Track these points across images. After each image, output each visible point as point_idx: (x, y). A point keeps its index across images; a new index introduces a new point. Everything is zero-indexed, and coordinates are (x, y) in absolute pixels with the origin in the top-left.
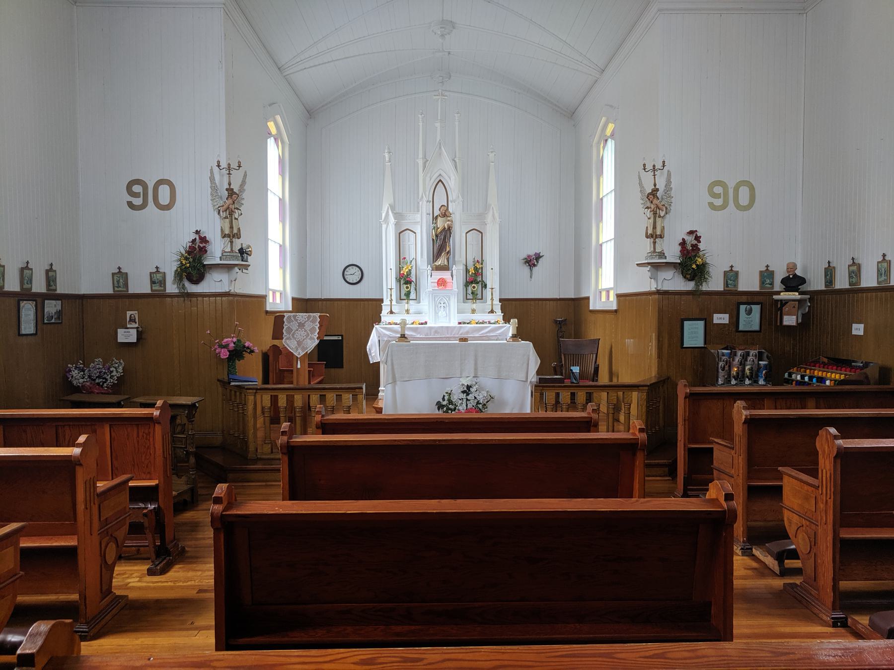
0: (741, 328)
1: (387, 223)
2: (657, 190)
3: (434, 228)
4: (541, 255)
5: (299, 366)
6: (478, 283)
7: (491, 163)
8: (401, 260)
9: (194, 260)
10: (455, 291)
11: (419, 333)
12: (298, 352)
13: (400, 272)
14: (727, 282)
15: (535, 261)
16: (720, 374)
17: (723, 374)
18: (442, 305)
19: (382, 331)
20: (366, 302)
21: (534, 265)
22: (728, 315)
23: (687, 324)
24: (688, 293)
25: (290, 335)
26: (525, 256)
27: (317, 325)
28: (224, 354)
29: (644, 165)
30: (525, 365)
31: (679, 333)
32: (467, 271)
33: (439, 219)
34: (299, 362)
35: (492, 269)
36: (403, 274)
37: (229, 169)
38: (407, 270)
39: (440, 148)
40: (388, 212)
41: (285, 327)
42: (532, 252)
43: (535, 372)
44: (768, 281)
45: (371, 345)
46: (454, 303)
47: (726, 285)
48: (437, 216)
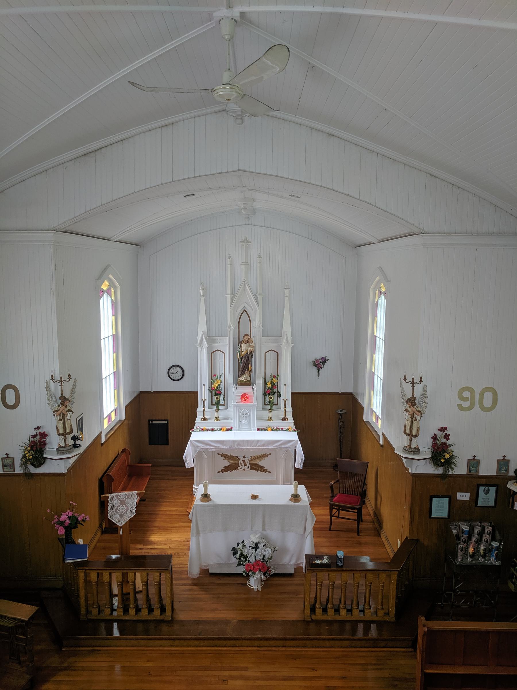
0: (480, 504)
2: (415, 399)
3: (239, 351)
5: (121, 533)
6: (273, 394)
7: (286, 298)
8: (212, 377)
9: (36, 453)
11: (225, 445)
12: (120, 522)
13: (212, 386)
14: (470, 468)
15: (321, 364)
16: (459, 553)
17: (461, 554)
18: (245, 415)
19: (195, 444)
20: (187, 394)
21: (321, 368)
22: (469, 493)
23: (434, 500)
24: (437, 476)
25: (114, 510)
26: (313, 359)
27: (134, 509)
28: (61, 532)
29: (405, 377)
30: (303, 522)
31: (428, 506)
32: (266, 383)
34: (121, 529)
35: (285, 385)
36: (214, 388)
37: (61, 382)
38: (217, 386)
39: (245, 285)
40: (202, 338)
41: (109, 505)
42: (318, 356)
43: (312, 528)
44: (504, 468)
45: (187, 455)
46: (254, 414)
47: (468, 471)
48: (242, 342)
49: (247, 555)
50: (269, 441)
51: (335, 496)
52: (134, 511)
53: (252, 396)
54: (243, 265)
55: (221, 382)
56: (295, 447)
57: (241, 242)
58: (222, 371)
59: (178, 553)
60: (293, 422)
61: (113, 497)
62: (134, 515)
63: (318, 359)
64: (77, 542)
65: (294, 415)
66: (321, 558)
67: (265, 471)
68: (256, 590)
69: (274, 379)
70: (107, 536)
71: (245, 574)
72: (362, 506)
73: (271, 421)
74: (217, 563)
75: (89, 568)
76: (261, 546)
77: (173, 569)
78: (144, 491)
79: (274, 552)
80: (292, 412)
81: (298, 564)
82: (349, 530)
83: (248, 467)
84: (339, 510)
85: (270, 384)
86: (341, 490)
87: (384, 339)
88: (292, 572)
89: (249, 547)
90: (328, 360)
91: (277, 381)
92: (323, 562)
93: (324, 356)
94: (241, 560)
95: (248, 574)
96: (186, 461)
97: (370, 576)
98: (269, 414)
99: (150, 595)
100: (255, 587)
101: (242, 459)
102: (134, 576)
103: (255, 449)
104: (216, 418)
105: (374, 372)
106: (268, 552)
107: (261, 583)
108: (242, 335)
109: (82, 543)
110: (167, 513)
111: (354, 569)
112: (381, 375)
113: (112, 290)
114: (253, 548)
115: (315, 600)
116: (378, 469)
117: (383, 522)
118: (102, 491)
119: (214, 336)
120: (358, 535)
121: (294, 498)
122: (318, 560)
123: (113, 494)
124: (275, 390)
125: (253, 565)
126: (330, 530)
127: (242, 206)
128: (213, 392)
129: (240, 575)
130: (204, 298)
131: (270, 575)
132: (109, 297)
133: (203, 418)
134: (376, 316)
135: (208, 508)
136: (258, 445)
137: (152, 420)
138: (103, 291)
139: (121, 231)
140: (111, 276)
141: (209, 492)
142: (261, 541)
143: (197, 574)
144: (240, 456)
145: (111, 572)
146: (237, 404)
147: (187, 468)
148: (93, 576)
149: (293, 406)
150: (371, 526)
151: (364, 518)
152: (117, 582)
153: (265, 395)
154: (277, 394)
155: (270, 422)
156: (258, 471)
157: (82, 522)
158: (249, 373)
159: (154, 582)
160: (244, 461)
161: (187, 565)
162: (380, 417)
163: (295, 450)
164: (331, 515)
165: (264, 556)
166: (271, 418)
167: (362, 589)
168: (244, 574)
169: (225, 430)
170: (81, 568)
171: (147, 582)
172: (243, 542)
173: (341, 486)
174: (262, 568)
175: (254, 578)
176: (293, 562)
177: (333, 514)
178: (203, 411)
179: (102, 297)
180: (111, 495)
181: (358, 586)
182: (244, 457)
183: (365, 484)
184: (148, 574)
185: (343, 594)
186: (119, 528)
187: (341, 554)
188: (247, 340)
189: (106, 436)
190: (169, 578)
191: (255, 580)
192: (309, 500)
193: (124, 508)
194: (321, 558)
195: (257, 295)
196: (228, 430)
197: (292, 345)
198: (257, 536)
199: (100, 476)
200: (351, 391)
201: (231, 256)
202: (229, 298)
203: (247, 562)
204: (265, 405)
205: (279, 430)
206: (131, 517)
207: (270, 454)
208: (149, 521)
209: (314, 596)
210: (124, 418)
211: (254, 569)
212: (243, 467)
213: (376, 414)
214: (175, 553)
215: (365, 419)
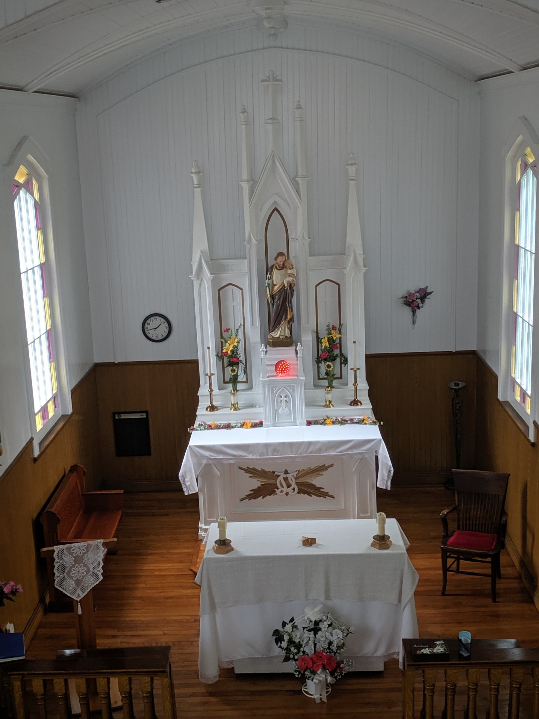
1: (200, 279)
3: (269, 285)
4: (428, 291)
5: (80, 612)
7: (351, 182)
10: (302, 380)
13: (222, 350)
15: (419, 301)
18: (283, 399)
19: (199, 452)
21: (419, 308)
25: (65, 574)
26: (403, 292)
27: (99, 571)
32: (319, 341)
33: (275, 272)
34: (79, 606)
35: (354, 342)
36: (227, 352)
38: (231, 348)
39: (274, 162)
41: (56, 566)
43: (413, 593)
45: (185, 472)
46: (299, 396)
48: (272, 267)
49: (299, 642)
50: (329, 442)
51: (452, 536)
52: (100, 574)
53: (294, 365)
54: (270, 123)
55: (238, 342)
56: (376, 452)
57: (263, 81)
58: (240, 321)
59: (179, 642)
60: (371, 407)
61: (61, 551)
62: (100, 580)
63: (412, 291)
64: (4, 629)
65: (371, 394)
66: (431, 644)
67: (325, 495)
68: (318, 701)
69: (333, 332)
70: (53, 617)
71: (298, 675)
72: (500, 552)
73: (330, 407)
74: (248, 657)
75: (29, 672)
76: (324, 626)
77: (173, 669)
78: (115, 539)
79: (347, 635)
80: (369, 391)
81: (389, 655)
82: (476, 594)
83: (294, 489)
84: (458, 559)
85: (326, 341)
86: (461, 523)
87: (533, 251)
88: (381, 668)
89: (304, 628)
90: (431, 293)
91: (340, 336)
92: (435, 651)
93: (423, 287)
94: (290, 650)
95: (303, 675)
96: (185, 482)
97: (519, 672)
98: (327, 395)
99: (135, 715)
100: (317, 696)
101: (282, 476)
102: (106, 684)
103: (304, 457)
104: (233, 405)
105: (516, 312)
106: (337, 636)
107: (327, 689)
108: (272, 255)
109: (12, 631)
110: (156, 573)
111: (491, 661)
112: (529, 316)
113: (34, 182)
114: (310, 631)
115: (422, 714)
116: (526, 485)
117: (537, 578)
118: (40, 542)
119: (222, 259)
120: (494, 601)
121: (379, 541)
122: (425, 648)
123: (61, 547)
124: (337, 352)
125: (312, 659)
126: (443, 594)
127: (263, 13)
128: (226, 360)
129: (289, 676)
130: (200, 189)
131: (342, 676)
132: (29, 196)
133: (209, 407)
134: (519, 209)
135: (229, 563)
136: (309, 451)
137: (119, 413)
138: (18, 186)
139: (43, 73)
140: (30, 157)
141: (228, 537)
142: (324, 618)
143: (214, 677)
144: (279, 470)
145: (67, 677)
146: (269, 380)
147: (186, 494)
148: (37, 685)
149: (369, 378)
150: (515, 585)
151: (503, 571)
152: (79, 695)
153: (318, 362)
154: (341, 360)
155: (330, 409)
156: (311, 496)
157: (11, 596)
158: (289, 323)
159: (143, 693)
160: (286, 479)
161: (196, 662)
162: (529, 392)
163: (377, 457)
164: (445, 569)
165: (330, 643)
166: (330, 402)
167: (505, 694)
168: (296, 674)
169: (249, 426)
170: (16, 673)
171: (130, 693)
172: (292, 620)
173: (461, 516)
174: (327, 664)
175: (314, 680)
176: (381, 652)
177: (448, 566)
178: (209, 394)
179: (18, 197)
180: (57, 548)
181: (497, 690)
182: (286, 472)
183: (503, 512)
184: (130, 679)
185: (471, 702)
186: (75, 604)
187: (466, 636)
188: (282, 263)
189: (40, 444)
190: (167, 686)
191: (315, 683)
192: (405, 544)
193: (82, 569)
194: (431, 644)
195: (297, 179)
196: (255, 425)
197: (364, 270)
198: (317, 610)
199: (35, 516)
200: (474, 348)
201: (246, 108)
202: (245, 186)
203: (301, 654)
204: (319, 379)
205: (346, 422)
206: (95, 584)
207: (332, 465)
208: (125, 589)
209: (421, 708)
210: (70, 410)
211: (313, 665)
212: (285, 490)
213: (522, 389)
214: (174, 643)
215: (500, 397)
